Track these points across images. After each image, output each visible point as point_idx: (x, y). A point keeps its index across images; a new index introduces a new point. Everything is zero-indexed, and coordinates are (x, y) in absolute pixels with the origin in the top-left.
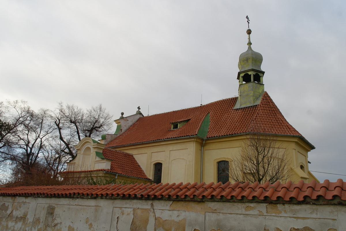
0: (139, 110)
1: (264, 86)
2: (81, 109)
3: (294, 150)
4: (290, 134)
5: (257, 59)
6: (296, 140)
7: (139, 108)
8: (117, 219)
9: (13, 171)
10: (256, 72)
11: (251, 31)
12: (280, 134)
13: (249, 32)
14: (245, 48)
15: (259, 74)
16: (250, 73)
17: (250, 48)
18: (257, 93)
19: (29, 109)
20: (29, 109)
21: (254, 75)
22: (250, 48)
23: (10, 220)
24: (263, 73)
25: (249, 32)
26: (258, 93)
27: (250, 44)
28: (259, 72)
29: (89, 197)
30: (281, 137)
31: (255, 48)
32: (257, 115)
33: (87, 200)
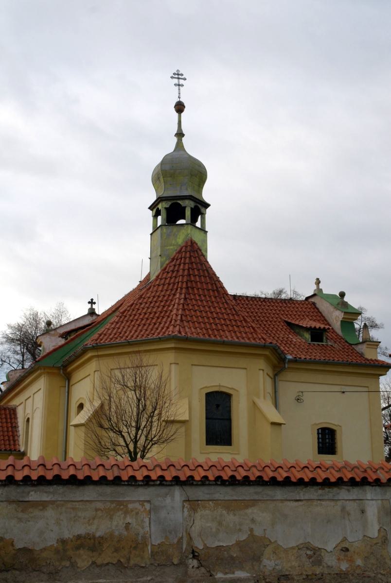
0: (92, 306)
1: (208, 233)
3: (261, 372)
4: (232, 337)
6: (172, 345)
7: (318, 282)
10: (171, 200)
11: (184, 107)
12: (195, 336)
13: (180, 108)
14: (170, 147)
15: (179, 202)
16: (182, 203)
17: (179, 146)
18: (172, 247)
21: (191, 208)
22: (179, 146)
23: (143, 552)
24: (207, 206)
25: (180, 108)
27: (180, 135)
29: (219, 483)
31: (192, 149)
32: (187, 296)
33: (349, 491)
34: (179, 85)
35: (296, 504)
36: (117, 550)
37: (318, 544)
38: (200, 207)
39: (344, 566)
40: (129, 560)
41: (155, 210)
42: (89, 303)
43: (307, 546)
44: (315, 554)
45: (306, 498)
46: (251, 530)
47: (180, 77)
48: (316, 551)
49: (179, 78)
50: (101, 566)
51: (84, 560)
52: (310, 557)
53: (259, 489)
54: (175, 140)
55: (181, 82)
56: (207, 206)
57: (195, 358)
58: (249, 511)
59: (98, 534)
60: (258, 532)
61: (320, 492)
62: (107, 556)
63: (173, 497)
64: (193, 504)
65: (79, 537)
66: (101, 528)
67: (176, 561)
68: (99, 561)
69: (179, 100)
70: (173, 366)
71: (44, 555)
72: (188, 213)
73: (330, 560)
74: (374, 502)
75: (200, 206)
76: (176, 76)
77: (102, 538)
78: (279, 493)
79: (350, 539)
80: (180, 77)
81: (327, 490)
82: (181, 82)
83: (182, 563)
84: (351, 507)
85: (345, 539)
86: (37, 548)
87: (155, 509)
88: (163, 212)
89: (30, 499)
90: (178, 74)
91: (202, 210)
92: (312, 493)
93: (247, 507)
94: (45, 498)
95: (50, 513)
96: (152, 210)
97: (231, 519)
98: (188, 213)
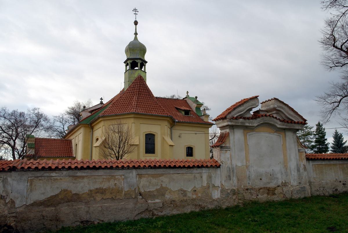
0: (101, 100)
2: (175, 95)
5: (143, 50)
7: (188, 93)
8: (266, 103)
9: (234, 129)
13: (136, 23)
14: (132, 38)
17: (136, 38)
18: (133, 78)
19: (70, 113)
20: (70, 113)
21: (140, 63)
22: (136, 38)
24: (146, 62)
25: (136, 23)
26: (133, 77)
27: (136, 34)
28: (135, 59)
30: (109, 116)
33: (197, 170)
34: (136, 14)
37: (185, 189)
39: (194, 197)
40: (116, 197)
41: (126, 63)
42: (100, 99)
44: (184, 192)
46: (162, 185)
47: (136, 11)
49: (136, 11)
51: (99, 197)
53: (165, 170)
54: (134, 36)
55: (137, 13)
56: (146, 62)
57: (141, 121)
60: (164, 185)
63: (132, 173)
64: (140, 176)
65: (97, 189)
66: (105, 185)
67: (133, 197)
68: (105, 198)
70: (133, 124)
71: (84, 196)
72: (139, 65)
73: (189, 195)
77: (105, 189)
78: (172, 171)
80: (136, 11)
81: (189, 170)
82: (137, 13)
83: (136, 198)
85: (195, 187)
87: (126, 178)
88: (129, 64)
89: (78, 175)
90: (135, 10)
91: (145, 64)
92: (184, 171)
93: (160, 176)
94: (84, 174)
95: (86, 180)
96: (125, 63)
97: (154, 181)
98: (139, 65)
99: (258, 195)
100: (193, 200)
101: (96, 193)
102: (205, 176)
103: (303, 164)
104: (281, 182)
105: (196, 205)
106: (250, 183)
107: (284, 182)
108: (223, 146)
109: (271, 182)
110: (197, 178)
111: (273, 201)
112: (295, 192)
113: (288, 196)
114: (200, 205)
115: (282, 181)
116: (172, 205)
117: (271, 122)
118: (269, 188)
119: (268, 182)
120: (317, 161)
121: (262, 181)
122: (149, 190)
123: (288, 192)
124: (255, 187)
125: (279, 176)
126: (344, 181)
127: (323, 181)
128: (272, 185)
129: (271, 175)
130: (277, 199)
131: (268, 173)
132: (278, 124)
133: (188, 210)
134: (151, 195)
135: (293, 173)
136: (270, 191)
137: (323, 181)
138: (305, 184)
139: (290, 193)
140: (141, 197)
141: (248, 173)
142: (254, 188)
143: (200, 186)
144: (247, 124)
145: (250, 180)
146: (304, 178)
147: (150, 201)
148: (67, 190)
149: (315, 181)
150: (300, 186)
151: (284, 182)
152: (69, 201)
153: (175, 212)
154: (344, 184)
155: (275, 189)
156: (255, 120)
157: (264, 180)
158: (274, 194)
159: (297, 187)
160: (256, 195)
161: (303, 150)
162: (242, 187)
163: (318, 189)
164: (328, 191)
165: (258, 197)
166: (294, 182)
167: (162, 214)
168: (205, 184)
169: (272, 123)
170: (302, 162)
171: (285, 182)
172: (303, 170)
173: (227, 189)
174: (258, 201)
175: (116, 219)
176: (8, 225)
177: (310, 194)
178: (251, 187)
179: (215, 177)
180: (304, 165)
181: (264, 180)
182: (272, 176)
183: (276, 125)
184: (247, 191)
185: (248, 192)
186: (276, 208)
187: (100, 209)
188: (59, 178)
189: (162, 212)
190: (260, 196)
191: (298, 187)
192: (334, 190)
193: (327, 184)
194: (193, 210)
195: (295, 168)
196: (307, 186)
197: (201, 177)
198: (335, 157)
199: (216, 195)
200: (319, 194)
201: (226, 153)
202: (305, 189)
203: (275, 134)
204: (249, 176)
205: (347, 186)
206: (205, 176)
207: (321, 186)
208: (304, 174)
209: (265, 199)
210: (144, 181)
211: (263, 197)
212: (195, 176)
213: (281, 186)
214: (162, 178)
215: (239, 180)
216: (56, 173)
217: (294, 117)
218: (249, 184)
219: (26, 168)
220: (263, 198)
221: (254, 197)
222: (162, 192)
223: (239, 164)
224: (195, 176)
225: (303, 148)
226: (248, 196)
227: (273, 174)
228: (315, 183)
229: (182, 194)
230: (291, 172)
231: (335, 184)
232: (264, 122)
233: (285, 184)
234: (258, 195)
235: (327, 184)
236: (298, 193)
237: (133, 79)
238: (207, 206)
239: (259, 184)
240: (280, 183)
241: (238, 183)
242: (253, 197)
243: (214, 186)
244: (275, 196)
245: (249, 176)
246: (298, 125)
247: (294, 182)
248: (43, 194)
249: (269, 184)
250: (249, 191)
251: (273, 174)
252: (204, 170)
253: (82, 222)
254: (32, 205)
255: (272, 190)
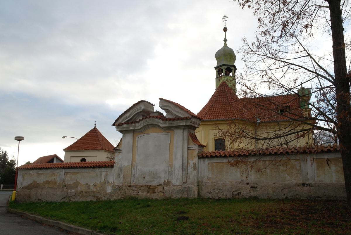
13: (225, 30)
17: (225, 45)
22: (225, 45)
25: (225, 30)
27: (225, 40)
31: (229, 45)
33: (98, 169)
35: (87, 173)
36: (52, 184)
37: (90, 184)
38: (219, 70)
39: (94, 190)
40: (54, 186)
43: (87, 184)
44: (88, 186)
45: (89, 171)
46: (77, 180)
48: (89, 185)
50: (49, 188)
51: (47, 186)
52: (88, 187)
53: (79, 169)
58: (77, 175)
59: (50, 180)
60: (78, 181)
61: (92, 170)
62: (50, 186)
63: (63, 171)
64: (66, 173)
65: (46, 181)
66: (50, 179)
67: (61, 187)
68: (49, 187)
69: (225, 27)
71: (41, 185)
73: (92, 188)
74: (104, 172)
75: (230, 67)
76: (224, 18)
77: (50, 181)
78: (83, 170)
79: (97, 183)
80: (226, 17)
81: (93, 169)
83: (63, 188)
84: (99, 174)
85: (96, 183)
86: (40, 183)
87: (60, 175)
89: (40, 172)
92: (90, 170)
93: (76, 174)
94: (42, 172)
95: (42, 176)
97: (73, 177)
99: (139, 192)
100: (94, 192)
101: (46, 183)
102: (103, 174)
103: (193, 162)
104: (164, 181)
105: (94, 196)
106: (134, 181)
107: (166, 181)
108: (117, 149)
109: (153, 181)
110: (98, 176)
111: (152, 198)
112: (175, 192)
113: (167, 195)
114: (97, 197)
115: (165, 180)
116: (81, 195)
117: (154, 123)
118: (150, 186)
119: (150, 181)
120: (215, 159)
121: (145, 179)
122: (70, 183)
123: (168, 191)
124: (138, 184)
125: (162, 175)
126: (254, 183)
127: (219, 182)
128: (154, 184)
129: (154, 174)
130: (156, 197)
131: (151, 172)
132: (160, 123)
133: (89, 199)
134: (69, 187)
135: (176, 172)
136: (151, 189)
137: (219, 182)
138: (192, 184)
139: (171, 192)
140: (66, 188)
141: (134, 172)
142: (137, 186)
143: (100, 182)
144: (131, 128)
145: (134, 178)
146: (191, 178)
147: (69, 191)
148: (35, 181)
149: (209, 182)
150: (184, 186)
151: (166, 181)
152: (35, 188)
153: (81, 200)
154: (252, 187)
155: (155, 187)
156: (138, 123)
157: (147, 178)
158: (154, 192)
159: (179, 186)
160: (137, 192)
161: (195, 147)
162: (126, 183)
163: (210, 191)
164: (225, 194)
165: (138, 194)
166: (176, 181)
167: (74, 200)
168: (102, 181)
169: (156, 123)
170: (193, 161)
171: (168, 181)
172: (192, 169)
173: (116, 185)
174: (137, 198)
175: (52, 200)
176: (139, 198)
177: (196, 195)
178: (134, 184)
179: (110, 175)
180: (195, 164)
181: (147, 178)
182: (155, 175)
183: (160, 124)
184: (129, 188)
185: (130, 189)
186: (279, 209)
187: (46, 193)
188: (33, 174)
189: (74, 199)
190: (140, 193)
191: (180, 186)
192: (235, 193)
193: (225, 186)
194: (92, 200)
195: (180, 167)
196: (195, 188)
197: (101, 175)
198: (40, 167)
199: (109, 190)
200: (212, 197)
201: (119, 154)
202: (191, 190)
203: (163, 133)
204: (134, 175)
205: (258, 189)
206: (103, 174)
207: (216, 188)
208: (193, 174)
209: (145, 196)
210: (68, 177)
211: (144, 194)
212: (97, 174)
213: (163, 184)
214: (79, 176)
215: (124, 178)
216: (32, 171)
217: (181, 113)
218: (133, 181)
219: (242, 154)
220: (143, 195)
221: (135, 194)
222: (77, 184)
223: (126, 164)
224: (97, 174)
225: (195, 145)
226: (129, 192)
227: (156, 173)
228: (207, 184)
229: (88, 187)
230: (174, 171)
231: (239, 187)
232: (148, 124)
233: (168, 183)
234: (139, 192)
235: (225, 186)
236: (178, 193)
237: (219, 84)
238: (102, 197)
239: (142, 182)
240: (162, 182)
241: (123, 180)
242: (134, 193)
243: (108, 182)
244: (155, 195)
245: (134, 175)
246: (181, 121)
247: (176, 181)
248: (27, 182)
249: (151, 182)
250: (132, 188)
251: (156, 173)
252: (103, 170)
253: (39, 200)
254: (23, 188)
255: (153, 188)
